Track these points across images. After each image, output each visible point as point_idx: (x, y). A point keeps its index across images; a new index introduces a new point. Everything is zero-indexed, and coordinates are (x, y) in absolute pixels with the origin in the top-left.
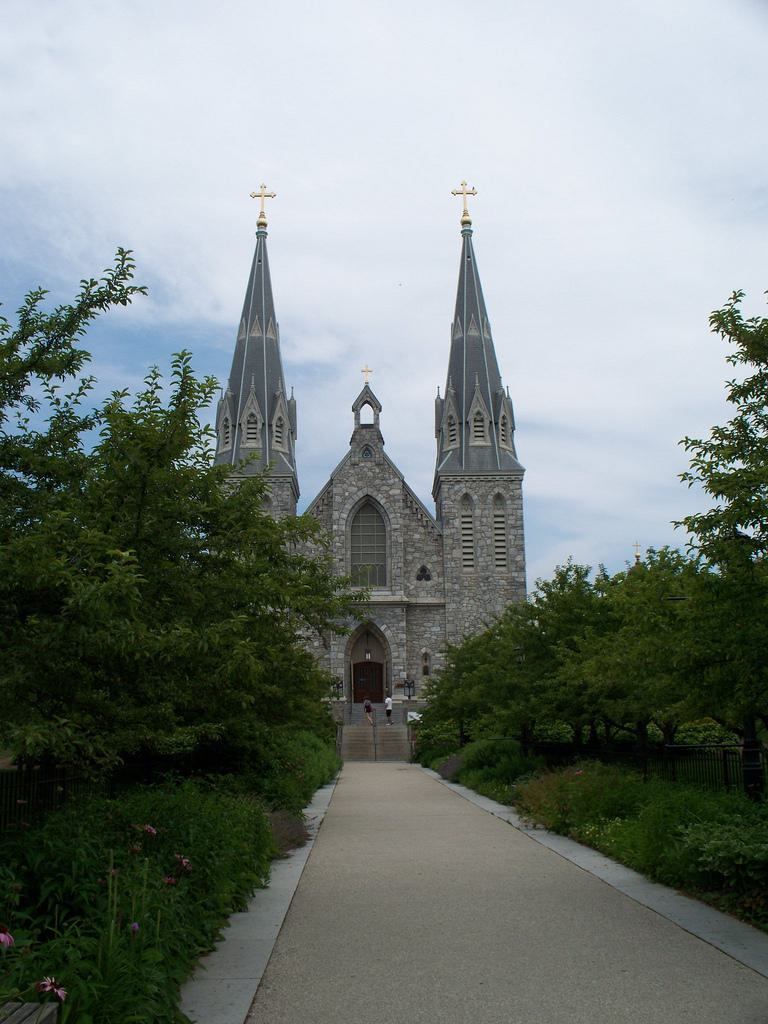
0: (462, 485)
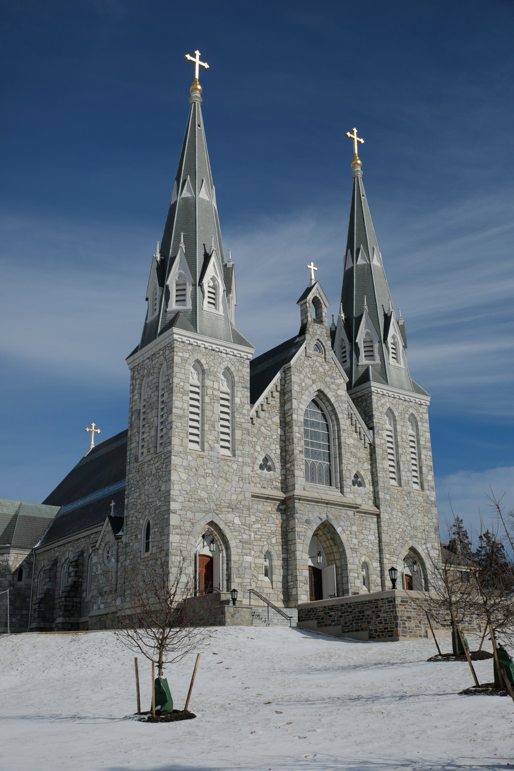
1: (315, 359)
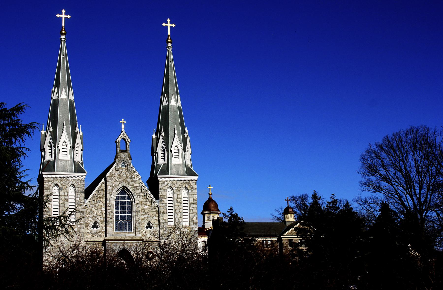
0: (168, 182)
1: (121, 171)
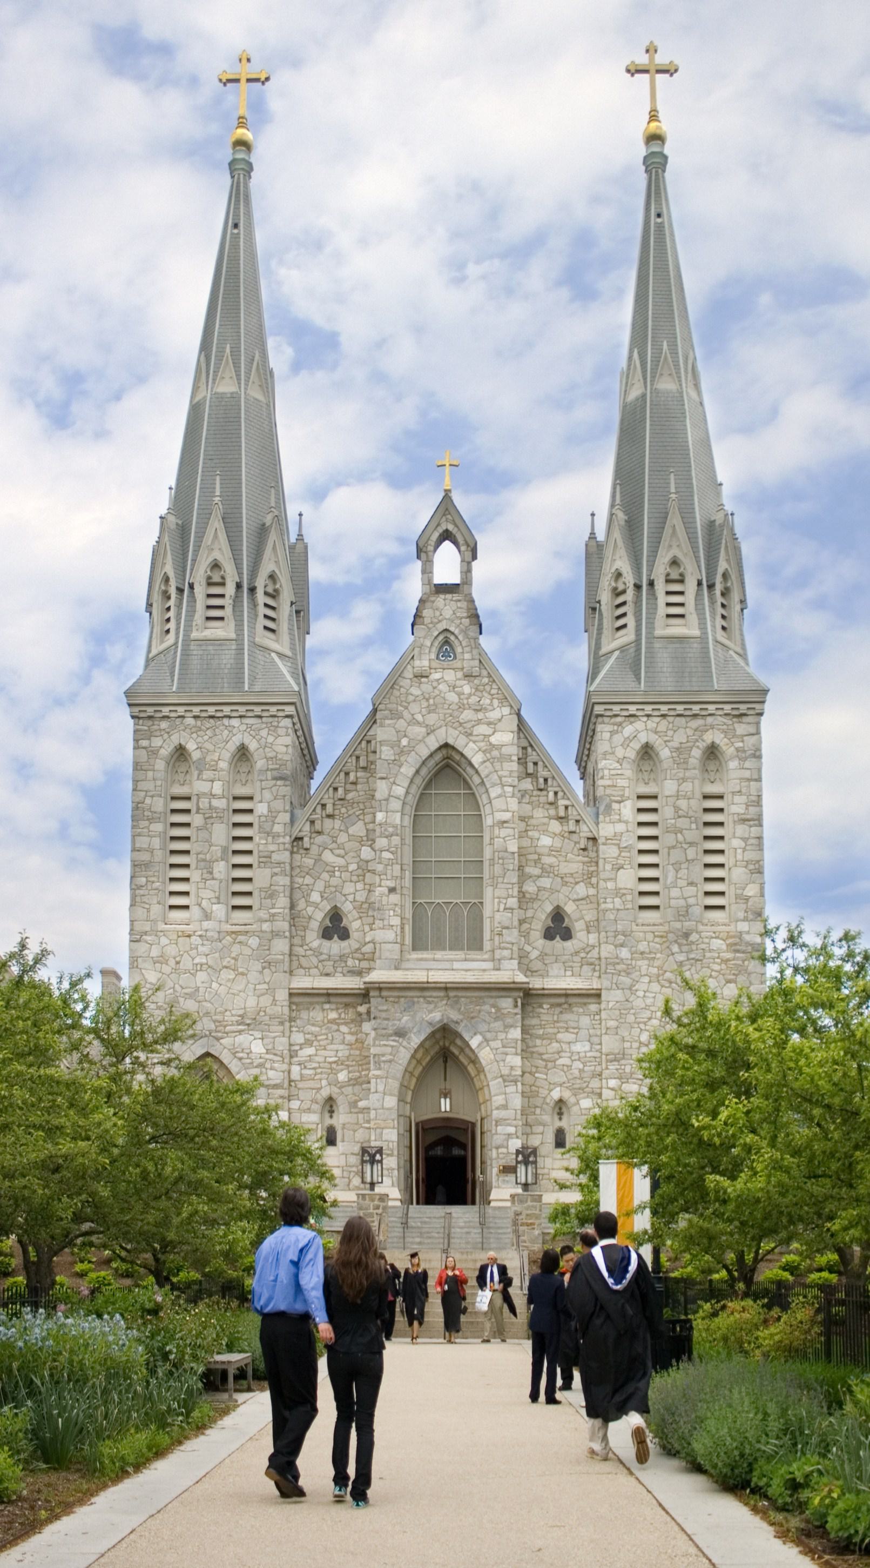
0: (639, 725)
